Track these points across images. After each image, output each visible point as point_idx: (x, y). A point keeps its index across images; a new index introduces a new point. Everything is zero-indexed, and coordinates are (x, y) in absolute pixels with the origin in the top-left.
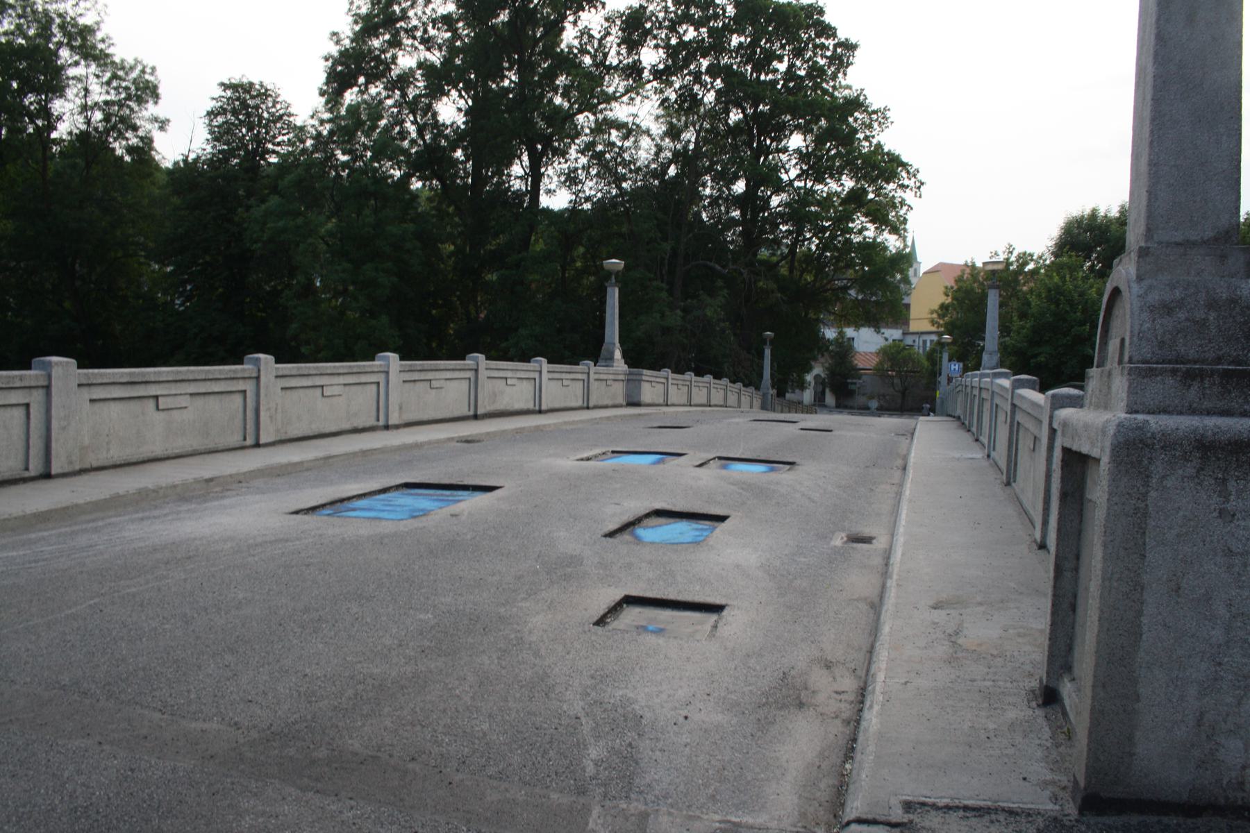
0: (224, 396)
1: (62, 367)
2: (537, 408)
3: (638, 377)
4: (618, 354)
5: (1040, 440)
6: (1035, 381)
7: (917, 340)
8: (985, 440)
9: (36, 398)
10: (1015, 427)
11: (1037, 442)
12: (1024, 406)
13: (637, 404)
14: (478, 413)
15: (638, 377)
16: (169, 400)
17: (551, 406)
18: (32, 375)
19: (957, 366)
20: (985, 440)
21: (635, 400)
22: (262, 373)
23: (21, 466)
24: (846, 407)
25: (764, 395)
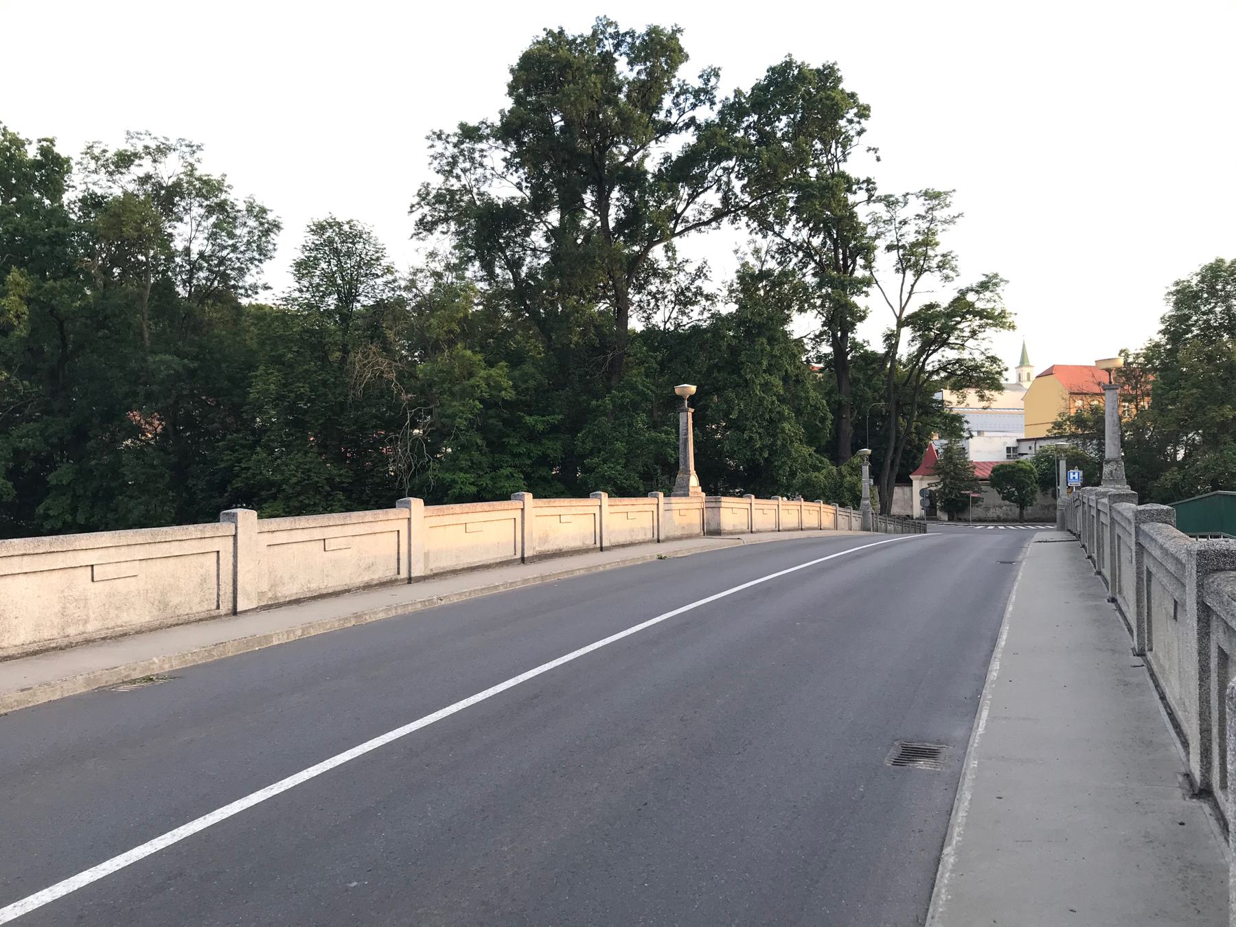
0: (65, 570)
1: (246, 517)
2: (519, 556)
3: (717, 505)
4: (694, 481)
5: (1184, 605)
6: (1168, 511)
7: (1033, 446)
8: (1106, 572)
9: (225, 546)
10: (1144, 580)
11: (1179, 608)
12: (1157, 553)
13: (717, 532)
14: (413, 575)
15: (717, 505)
16: (109, 568)
17: (614, 541)
18: (224, 527)
19: (1077, 474)
20: (1106, 572)
21: (713, 527)
22: (239, 530)
23: (214, 607)
24: (960, 520)
25: (865, 514)
